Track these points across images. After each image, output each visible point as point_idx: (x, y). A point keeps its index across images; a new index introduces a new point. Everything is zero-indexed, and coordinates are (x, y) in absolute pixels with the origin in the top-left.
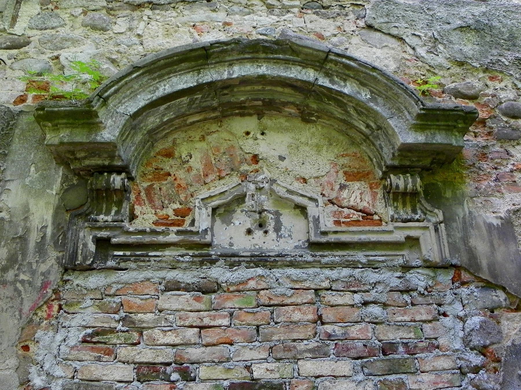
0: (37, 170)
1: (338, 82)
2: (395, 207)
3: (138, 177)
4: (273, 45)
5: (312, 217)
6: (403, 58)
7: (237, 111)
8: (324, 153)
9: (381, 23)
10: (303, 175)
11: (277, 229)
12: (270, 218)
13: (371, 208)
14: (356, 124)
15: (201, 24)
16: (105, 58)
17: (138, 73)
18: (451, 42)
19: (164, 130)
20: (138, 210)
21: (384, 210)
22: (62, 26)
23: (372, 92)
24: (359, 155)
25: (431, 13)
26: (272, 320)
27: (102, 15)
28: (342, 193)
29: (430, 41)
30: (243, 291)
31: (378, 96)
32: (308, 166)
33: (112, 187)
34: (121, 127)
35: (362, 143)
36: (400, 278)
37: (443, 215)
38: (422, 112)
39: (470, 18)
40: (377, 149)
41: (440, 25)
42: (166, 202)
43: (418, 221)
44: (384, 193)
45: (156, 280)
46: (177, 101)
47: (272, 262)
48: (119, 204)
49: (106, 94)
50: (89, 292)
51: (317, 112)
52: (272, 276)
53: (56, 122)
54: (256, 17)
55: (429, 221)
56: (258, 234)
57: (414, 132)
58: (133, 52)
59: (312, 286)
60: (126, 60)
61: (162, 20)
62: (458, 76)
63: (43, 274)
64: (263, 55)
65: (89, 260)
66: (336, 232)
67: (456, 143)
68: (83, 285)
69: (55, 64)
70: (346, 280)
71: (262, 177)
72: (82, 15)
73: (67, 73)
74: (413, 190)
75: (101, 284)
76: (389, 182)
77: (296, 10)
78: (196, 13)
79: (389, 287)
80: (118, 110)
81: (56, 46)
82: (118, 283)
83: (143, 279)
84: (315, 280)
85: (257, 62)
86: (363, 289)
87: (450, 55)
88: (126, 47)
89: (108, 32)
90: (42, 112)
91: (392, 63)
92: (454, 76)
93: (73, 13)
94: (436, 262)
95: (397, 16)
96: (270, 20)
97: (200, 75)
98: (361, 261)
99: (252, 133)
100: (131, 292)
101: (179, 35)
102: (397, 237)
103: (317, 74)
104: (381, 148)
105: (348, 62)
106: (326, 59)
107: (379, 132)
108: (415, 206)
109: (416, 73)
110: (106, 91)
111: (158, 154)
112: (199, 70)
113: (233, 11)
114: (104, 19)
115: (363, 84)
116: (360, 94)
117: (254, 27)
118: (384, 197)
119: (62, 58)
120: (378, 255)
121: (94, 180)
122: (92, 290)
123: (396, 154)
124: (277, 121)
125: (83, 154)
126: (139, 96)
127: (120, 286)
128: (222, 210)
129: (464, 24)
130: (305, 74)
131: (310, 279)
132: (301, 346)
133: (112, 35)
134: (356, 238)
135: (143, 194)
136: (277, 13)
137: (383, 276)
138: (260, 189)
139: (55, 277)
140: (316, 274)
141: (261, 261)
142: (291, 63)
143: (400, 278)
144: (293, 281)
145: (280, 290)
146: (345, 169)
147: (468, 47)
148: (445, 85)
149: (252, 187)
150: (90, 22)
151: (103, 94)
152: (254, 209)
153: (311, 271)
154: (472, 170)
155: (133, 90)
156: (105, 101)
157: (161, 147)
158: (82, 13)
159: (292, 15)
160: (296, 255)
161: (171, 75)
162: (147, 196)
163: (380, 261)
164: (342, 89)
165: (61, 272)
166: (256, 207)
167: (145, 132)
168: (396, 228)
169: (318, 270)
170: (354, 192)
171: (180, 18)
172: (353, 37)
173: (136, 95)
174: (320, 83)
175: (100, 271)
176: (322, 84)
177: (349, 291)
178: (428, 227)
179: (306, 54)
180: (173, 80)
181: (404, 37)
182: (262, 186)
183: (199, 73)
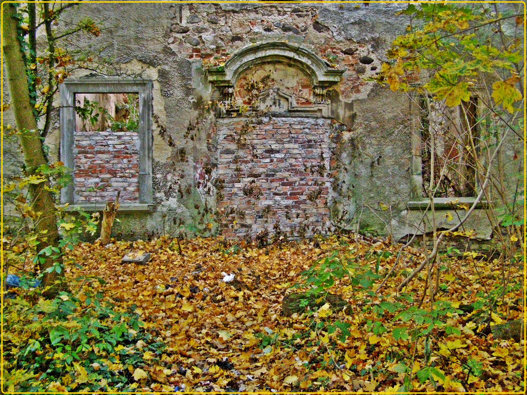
11: (279, 105)
21: (312, 99)
26: (276, 133)
48: (231, 97)
54: (273, 17)
56: (273, 107)
77: (289, 13)
106: (298, 50)
120: (309, 114)
132: (285, 140)
134: (303, 109)
139: (214, 120)
145: (279, 124)
147: (354, 32)
149: (272, 91)
153: (289, 118)
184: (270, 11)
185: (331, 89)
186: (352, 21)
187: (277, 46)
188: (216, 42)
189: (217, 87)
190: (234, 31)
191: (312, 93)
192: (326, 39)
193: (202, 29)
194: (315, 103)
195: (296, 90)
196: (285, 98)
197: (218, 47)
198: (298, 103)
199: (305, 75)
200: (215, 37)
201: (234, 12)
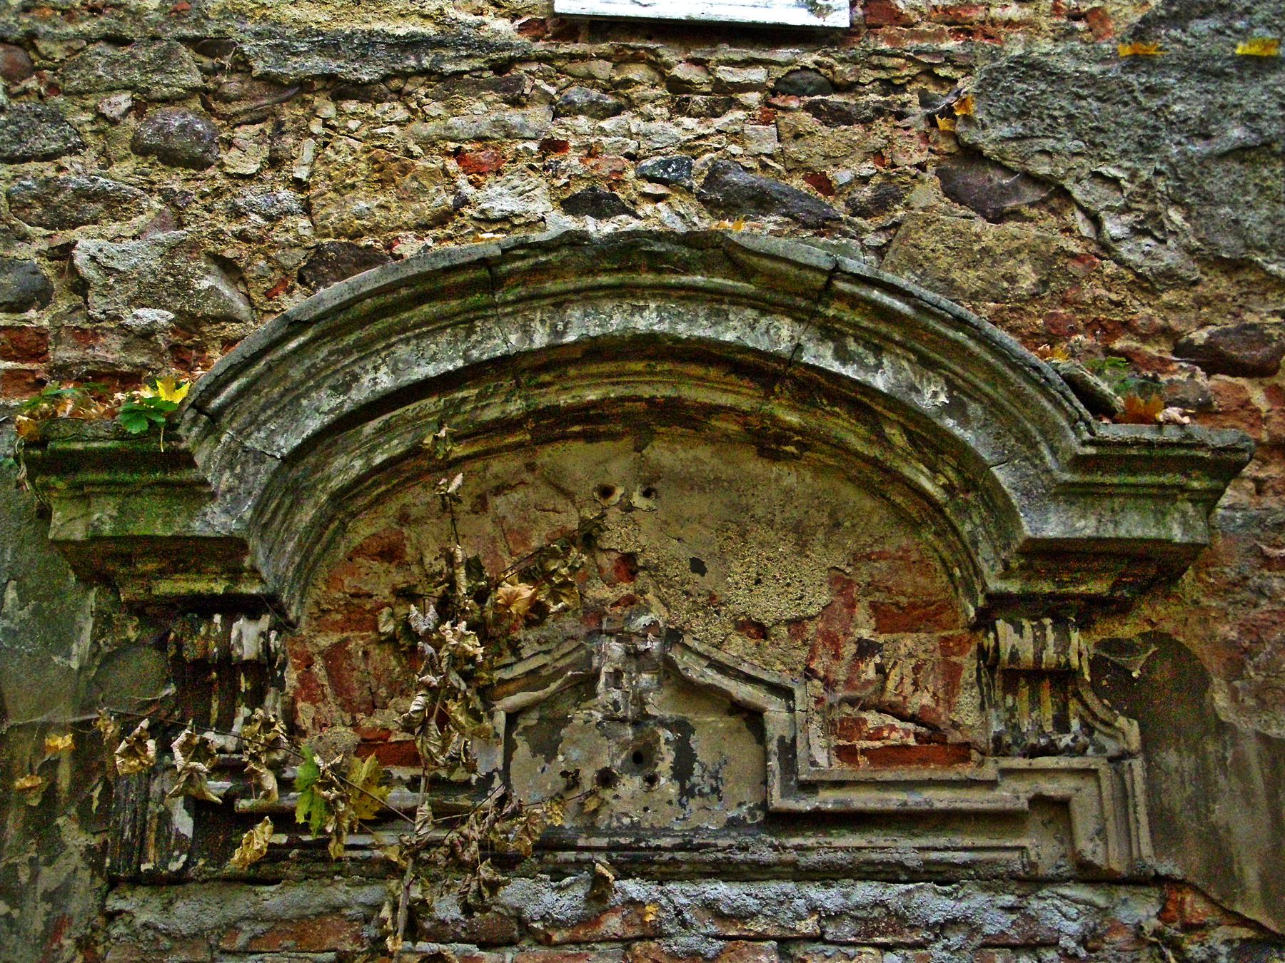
0: (23, 599)
1: (859, 355)
2: (1008, 710)
3: (304, 619)
4: (676, 248)
5: (775, 742)
6: (1063, 252)
7: (576, 428)
8: (818, 548)
9: (1005, 139)
10: (757, 615)
11: (682, 771)
12: (662, 741)
13: (941, 710)
14: (907, 471)
15: (478, 146)
16: (203, 257)
17: (302, 339)
18: (1207, 198)
19: (376, 484)
20: (306, 713)
22: (73, 151)
23: (951, 385)
24: (915, 556)
25: (1155, 103)
27: (190, 117)
28: (862, 667)
29: (1144, 196)
30: (588, 942)
31: (970, 397)
32: (770, 588)
33: (234, 655)
34: (257, 492)
35: (924, 522)
36: (1010, 909)
37: (1142, 733)
38: (1090, 450)
39: (1273, 118)
40: (965, 546)
41: (1179, 143)
42: (383, 692)
43: (1070, 751)
44: (978, 670)
45: (356, 911)
46: (411, 407)
47: (666, 864)
49: (215, 403)
50: (177, 945)
51: (798, 433)
52: (664, 901)
53: (80, 477)
54: (636, 124)
55: (1100, 749)
56: (630, 785)
57: (1063, 506)
58: (282, 238)
59: (772, 932)
60: (262, 263)
61: (364, 132)
62: (1220, 305)
63: (49, 896)
64: (648, 278)
65: (177, 859)
66: (838, 784)
67: (1185, 532)
68: (161, 926)
69: (61, 273)
70: (864, 914)
71: (644, 620)
72: (132, 115)
73: (97, 305)
74: (1059, 664)
75: (210, 922)
76: (992, 643)
78: (463, 111)
79: (980, 937)
80: (248, 444)
81: (59, 215)
82: (254, 918)
83: (321, 909)
84: (781, 915)
85: (633, 296)
86: (909, 941)
87: (1200, 240)
88: (260, 220)
89: (210, 172)
90: (38, 452)
91: (1027, 268)
92: (1208, 304)
93: (106, 110)
94: (1111, 870)
95: (1051, 116)
96: (676, 131)
97: (474, 337)
98: (907, 864)
99: (619, 491)
100: (290, 943)
101: (415, 184)
102: (1005, 800)
103: (799, 328)
104: (975, 543)
105: (887, 300)
107: (971, 497)
108: (1066, 705)
109: (1095, 299)
110: (216, 394)
111: (359, 551)
112: (472, 321)
113: (572, 103)
114: (197, 133)
115: (926, 363)
116: (918, 391)
117: (630, 156)
118: (979, 678)
119: (80, 259)
121: (179, 625)
122: (184, 937)
123: (1014, 564)
124: (691, 453)
125: (152, 566)
126: (304, 402)
127: (260, 928)
128: (532, 719)
129: (1252, 139)
130: (767, 331)
131: (766, 911)
133: (222, 182)
134: (894, 800)
135: (318, 668)
136: (697, 109)
137: (964, 904)
138: (633, 655)
140: (782, 898)
141: (634, 860)
142: (726, 300)
143: (1010, 909)
144: (720, 916)
146: (878, 597)
148: (1180, 334)
149: (616, 649)
150: (157, 140)
151: (208, 402)
152: (620, 714)
153: (772, 888)
154: (1238, 597)
155: (288, 385)
156: (214, 422)
157: (368, 531)
158: (129, 110)
159: (740, 114)
160: (731, 846)
161: (394, 339)
162: (329, 674)
163: (956, 865)
164: (870, 379)
165: (100, 889)
166: (626, 707)
167: (324, 498)
168: (1006, 772)
169: (789, 887)
170: (895, 663)
171: (418, 127)
172: (918, 187)
173: (298, 398)
174: (807, 358)
175: (206, 886)
176: (812, 361)
177: (869, 945)
178: (1096, 771)
179: (773, 276)
180: (399, 352)
181: (1068, 184)
182: (642, 647)
183: (470, 331)
184: (613, 87)
185: (1127, 630)
186: (1237, 133)
187: (656, 262)
188: (183, 287)
189: (136, 609)
190: (332, 214)
191: (968, 664)
192: (1050, 262)
193: (84, 194)
194: (999, 748)
195: (832, 640)
196: (738, 708)
197: (188, 323)
198: (847, 754)
199: (901, 518)
200: (173, 249)
201: (340, 89)
